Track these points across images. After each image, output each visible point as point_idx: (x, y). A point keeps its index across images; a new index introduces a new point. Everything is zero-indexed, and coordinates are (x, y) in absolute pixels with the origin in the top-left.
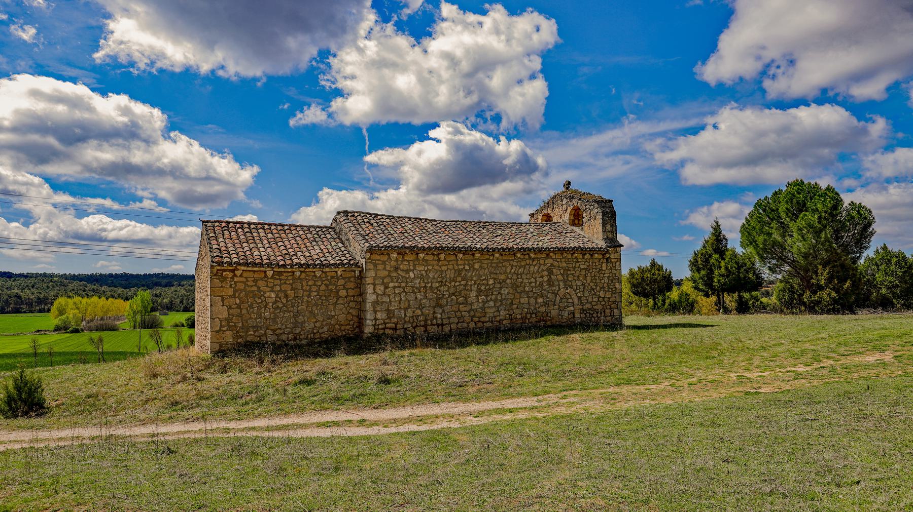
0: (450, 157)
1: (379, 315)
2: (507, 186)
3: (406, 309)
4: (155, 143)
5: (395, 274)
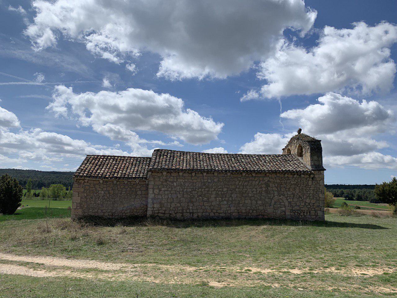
0: (330, 112)
1: (155, 206)
2: (363, 129)
3: (171, 203)
4: (179, 114)
5: (165, 184)
